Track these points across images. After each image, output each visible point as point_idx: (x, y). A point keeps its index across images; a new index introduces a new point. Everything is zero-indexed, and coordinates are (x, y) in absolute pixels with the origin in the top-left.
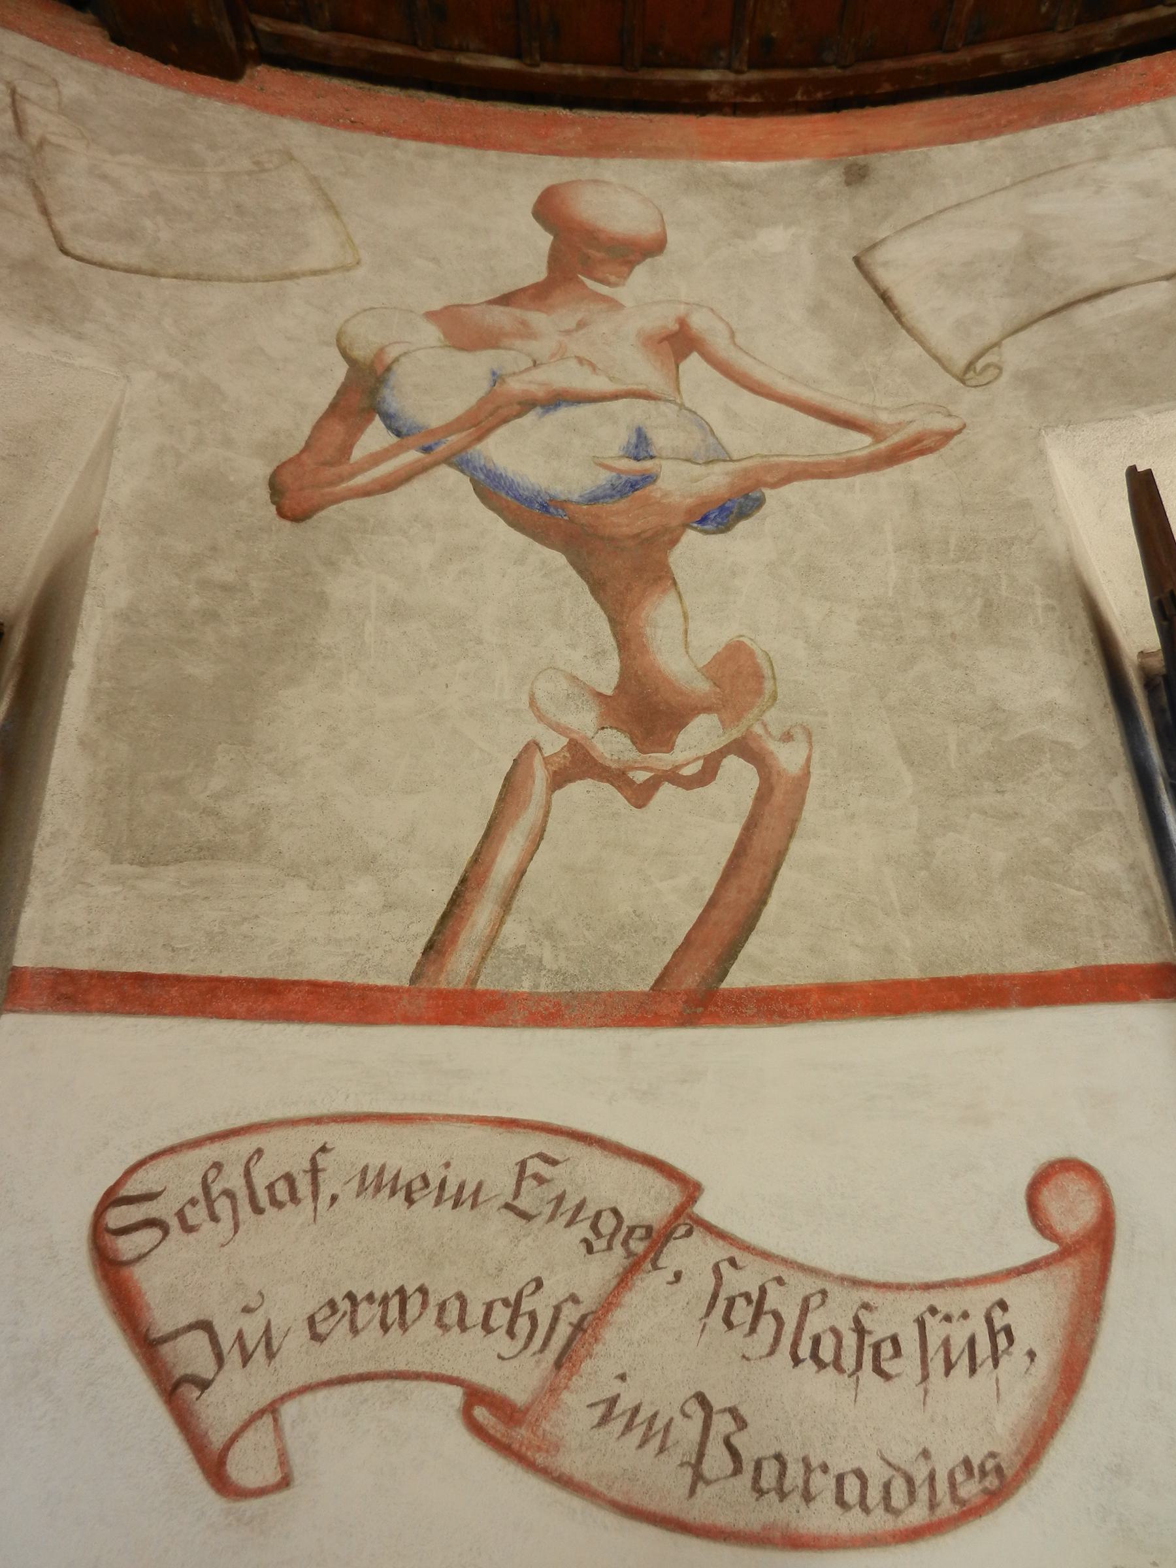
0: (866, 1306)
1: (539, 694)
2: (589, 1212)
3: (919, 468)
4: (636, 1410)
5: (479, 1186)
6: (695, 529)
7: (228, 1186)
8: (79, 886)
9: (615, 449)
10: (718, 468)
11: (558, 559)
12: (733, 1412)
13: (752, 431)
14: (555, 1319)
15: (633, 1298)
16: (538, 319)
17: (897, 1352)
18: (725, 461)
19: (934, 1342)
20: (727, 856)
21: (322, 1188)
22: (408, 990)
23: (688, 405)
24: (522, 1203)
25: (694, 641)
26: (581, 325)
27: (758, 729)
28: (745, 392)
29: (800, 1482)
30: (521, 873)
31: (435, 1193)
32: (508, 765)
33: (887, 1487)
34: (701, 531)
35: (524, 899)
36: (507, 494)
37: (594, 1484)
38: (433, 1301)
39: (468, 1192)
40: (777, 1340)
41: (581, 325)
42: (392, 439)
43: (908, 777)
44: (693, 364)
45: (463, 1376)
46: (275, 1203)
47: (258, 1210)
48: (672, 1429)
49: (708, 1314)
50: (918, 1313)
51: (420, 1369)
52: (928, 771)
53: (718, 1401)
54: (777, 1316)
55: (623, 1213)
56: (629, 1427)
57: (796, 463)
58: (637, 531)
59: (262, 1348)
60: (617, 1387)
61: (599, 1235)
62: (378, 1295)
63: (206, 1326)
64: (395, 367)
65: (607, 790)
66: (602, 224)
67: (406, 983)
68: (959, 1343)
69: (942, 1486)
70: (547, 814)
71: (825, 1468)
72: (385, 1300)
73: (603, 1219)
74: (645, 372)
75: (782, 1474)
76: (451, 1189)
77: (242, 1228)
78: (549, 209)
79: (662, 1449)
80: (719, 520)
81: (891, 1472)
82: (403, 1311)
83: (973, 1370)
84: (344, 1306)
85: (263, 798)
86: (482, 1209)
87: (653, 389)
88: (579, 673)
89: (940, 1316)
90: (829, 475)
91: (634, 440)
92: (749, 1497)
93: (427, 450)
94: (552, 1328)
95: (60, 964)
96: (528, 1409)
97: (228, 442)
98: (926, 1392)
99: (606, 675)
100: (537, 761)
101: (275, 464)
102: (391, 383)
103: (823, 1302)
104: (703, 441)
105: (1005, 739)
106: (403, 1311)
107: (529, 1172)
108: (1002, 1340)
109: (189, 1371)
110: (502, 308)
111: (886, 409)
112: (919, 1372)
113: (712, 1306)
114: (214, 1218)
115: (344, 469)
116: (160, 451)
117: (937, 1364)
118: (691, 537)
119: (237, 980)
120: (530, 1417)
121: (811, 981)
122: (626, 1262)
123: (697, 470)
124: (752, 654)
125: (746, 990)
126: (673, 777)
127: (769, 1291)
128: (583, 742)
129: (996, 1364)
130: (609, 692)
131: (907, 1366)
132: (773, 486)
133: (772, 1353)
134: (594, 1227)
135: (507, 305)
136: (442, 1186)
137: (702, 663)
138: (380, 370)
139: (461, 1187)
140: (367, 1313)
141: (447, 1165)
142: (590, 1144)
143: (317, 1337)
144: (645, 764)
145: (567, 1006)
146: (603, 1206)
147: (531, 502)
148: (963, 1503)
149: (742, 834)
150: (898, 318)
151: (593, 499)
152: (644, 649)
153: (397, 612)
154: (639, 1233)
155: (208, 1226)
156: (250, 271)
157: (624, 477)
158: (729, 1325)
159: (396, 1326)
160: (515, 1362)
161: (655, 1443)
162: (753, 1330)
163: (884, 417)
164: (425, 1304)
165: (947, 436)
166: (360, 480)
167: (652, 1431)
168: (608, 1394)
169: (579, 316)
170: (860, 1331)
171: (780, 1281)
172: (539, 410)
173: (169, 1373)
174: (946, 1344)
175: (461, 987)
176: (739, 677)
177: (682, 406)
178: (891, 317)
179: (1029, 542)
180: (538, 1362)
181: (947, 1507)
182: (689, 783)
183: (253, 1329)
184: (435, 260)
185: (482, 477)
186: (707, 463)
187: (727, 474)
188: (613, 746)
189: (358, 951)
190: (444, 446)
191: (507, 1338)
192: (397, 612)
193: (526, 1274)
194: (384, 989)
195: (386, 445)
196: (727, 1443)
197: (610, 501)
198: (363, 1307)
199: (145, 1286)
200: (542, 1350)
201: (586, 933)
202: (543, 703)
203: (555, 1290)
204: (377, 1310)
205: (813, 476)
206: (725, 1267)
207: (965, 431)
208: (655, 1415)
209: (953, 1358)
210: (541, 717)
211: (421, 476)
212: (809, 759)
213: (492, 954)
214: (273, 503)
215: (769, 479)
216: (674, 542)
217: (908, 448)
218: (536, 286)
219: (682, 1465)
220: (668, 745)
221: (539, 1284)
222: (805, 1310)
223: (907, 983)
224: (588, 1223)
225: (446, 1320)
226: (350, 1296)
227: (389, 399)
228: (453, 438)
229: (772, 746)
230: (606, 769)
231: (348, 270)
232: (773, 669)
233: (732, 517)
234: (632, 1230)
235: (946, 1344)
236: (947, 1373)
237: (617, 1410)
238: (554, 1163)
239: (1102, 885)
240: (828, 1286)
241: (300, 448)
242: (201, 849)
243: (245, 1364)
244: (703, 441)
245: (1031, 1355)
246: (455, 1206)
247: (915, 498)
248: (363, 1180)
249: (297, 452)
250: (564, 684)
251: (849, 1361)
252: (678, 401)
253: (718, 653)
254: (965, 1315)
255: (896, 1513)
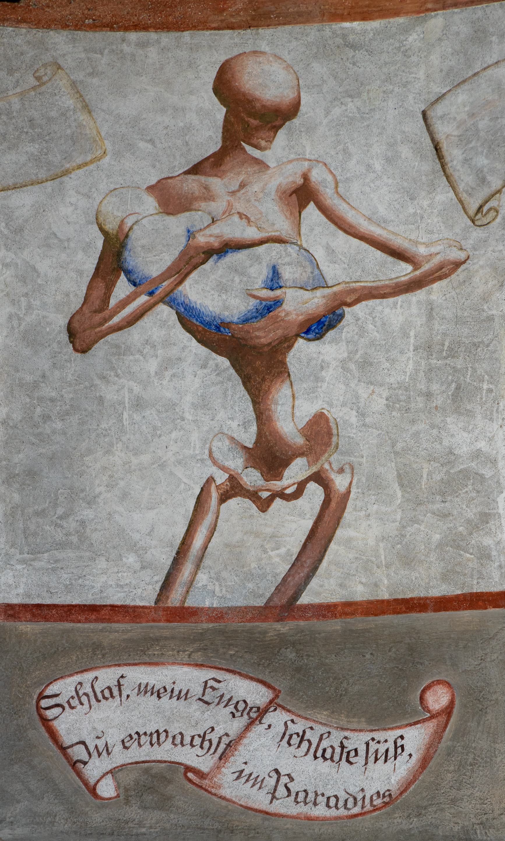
0: (346, 738)
1: (214, 449)
2: (234, 701)
3: (437, 291)
4: (251, 775)
5: (188, 691)
6: (302, 337)
7: (86, 691)
8: (8, 566)
9: (259, 283)
10: (319, 293)
11: (224, 362)
12: (289, 775)
13: (341, 260)
14: (219, 742)
15: (251, 735)
16: (216, 183)
17: (356, 755)
18: (324, 287)
19: (372, 750)
20: (305, 537)
21: (123, 692)
22: (154, 607)
23: (305, 246)
24: (206, 698)
25: (297, 414)
26: (242, 186)
27: (327, 466)
28: (341, 232)
29: (313, 799)
30: (205, 547)
31: (169, 694)
32: (198, 491)
33: (346, 801)
34: (305, 339)
35: (207, 562)
36: (197, 320)
37: (234, 799)
38: (170, 735)
39: (183, 694)
40: (308, 750)
41: (242, 186)
42: (132, 288)
43: (399, 494)
44: (311, 211)
45: (183, 762)
46: (105, 698)
47: (98, 701)
48: (265, 781)
49: (281, 741)
50: (367, 740)
51: (166, 760)
52: (410, 490)
53: (283, 772)
54: (309, 741)
55: (248, 702)
56: (247, 780)
57: (365, 287)
58: (269, 341)
59: (105, 751)
60: (243, 766)
61: (237, 711)
62: (148, 733)
63: (83, 743)
64: (130, 234)
65: (247, 503)
66: (258, 93)
67: (153, 604)
68: (382, 751)
69: (367, 801)
70: (217, 518)
71: (323, 795)
72: (151, 734)
73: (239, 704)
74: (280, 223)
75: (306, 797)
76: (176, 693)
77: (93, 707)
78: (224, 86)
79: (260, 788)
80: (317, 331)
81: (348, 796)
82: (158, 739)
83: (386, 761)
84: (135, 736)
85: (82, 517)
86: (189, 700)
87: (284, 235)
88: (235, 436)
89: (376, 741)
90: (384, 296)
91: (270, 276)
92: (293, 804)
93: (151, 294)
94: (218, 745)
95: (6, 601)
96: (208, 774)
97: (44, 305)
98: (366, 769)
99: (249, 437)
100: (213, 488)
101: (70, 316)
102: (129, 247)
103: (329, 736)
104: (312, 273)
105: (452, 471)
106: (158, 739)
107: (208, 685)
108: (399, 750)
109: (79, 758)
110: (193, 177)
111: (424, 243)
112: (364, 762)
113: (283, 737)
114: (82, 704)
115: (106, 313)
116: (10, 317)
117: (372, 759)
118: (300, 342)
119: (79, 606)
120: (209, 777)
121: (339, 600)
122: (249, 721)
123: (307, 295)
124: (327, 420)
125: (308, 605)
126: (282, 495)
127: (307, 732)
128: (236, 476)
129: (395, 759)
130: (251, 446)
131: (360, 760)
132: (349, 305)
133: (306, 755)
134: (236, 707)
135: (196, 174)
136: (172, 691)
137: (301, 426)
138: (122, 238)
139: (180, 692)
140: (143, 739)
141: (174, 683)
142: (235, 674)
143: (125, 748)
144: (268, 488)
145: (226, 614)
146: (240, 699)
147: (210, 325)
148: (375, 806)
149: (313, 526)
150: (443, 166)
151: (246, 320)
152: (270, 419)
153: (138, 404)
154: (254, 710)
155: (79, 707)
156: (42, 175)
157: (264, 303)
158: (290, 745)
159: (156, 744)
160: (203, 757)
161: (258, 786)
162: (299, 746)
163: (422, 250)
164: (167, 736)
165: (457, 264)
166: (116, 320)
167: (257, 782)
168: (240, 769)
169: (241, 178)
170: (342, 747)
171: (311, 728)
172: (215, 257)
173: (72, 760)
174: (377, 751)
175: (178, 605)
176: (320, 433)
177: (301, 247)
178: (439, 166)
179: (488, 346)
180: (212, 758)
181: (368, 807)
182: (288, 498)
183: (101, 744)
184: (151, 141)
185: (183, 310)
186: (313, 289)
187: (324, 297)
188: (252, 478)
189: (131, 590)
190: (160, 290)
191: (200, 749)
192: (138, 404)
193: (207, 725)
194: (143, 607)
195: (128, 293)
196: (286, 786)
197: (256, 320)
198: (143, 737)
199: (59, 728)
200: (214, 753)
201: (235, 578)
202: (217, 455)
203: (220, 730)
204: (148, 738)
205: (374, 297)
206: (289, 723)
207: (468, 262)
208: (258, 776)
209: (379, 757)
210: (215, 462)
211: (148, 313)
212: (351, 483)
213: (191, 589)
214: (71, 342)
215: (349, 300)
216: (290, 347)
217: (433, 274)
218: (214, 155)
219: (268, 793)
220: (278, 476)
221: (213, 729)
222: (321, 739)
223: (383, 601)
224: (233, 706)
225: (176, 742)
226: (137, 733)
227: (128, 259)
228: (165, 284)
229: (333, 476)
230: (248, 491)
231: (99, 160)
232: (338, 429)
233: (324, 328)
234: (251, 708)
235: (377, 751)
236: (375, 762)
237: (243, 775)
238: (219, 682)
239: (483, 552)
240: (331, 730)
241: (82, 303)
242: (57, 544)
243: (99, 757)
244: (312, 273)
245: (410, 755)
246: (178, 699)
247: (431, 311)
248: (139, 689)
249: (80, 306)
250: (227, 442)
251: (336, 757)
252: (299, 243)
253: (310, 420)
254: (386, 741)
255: (349, 809)
